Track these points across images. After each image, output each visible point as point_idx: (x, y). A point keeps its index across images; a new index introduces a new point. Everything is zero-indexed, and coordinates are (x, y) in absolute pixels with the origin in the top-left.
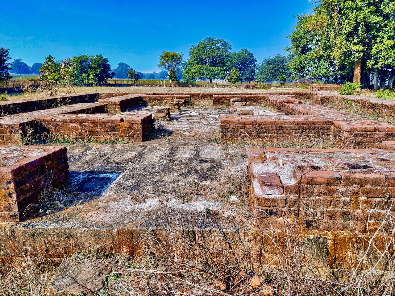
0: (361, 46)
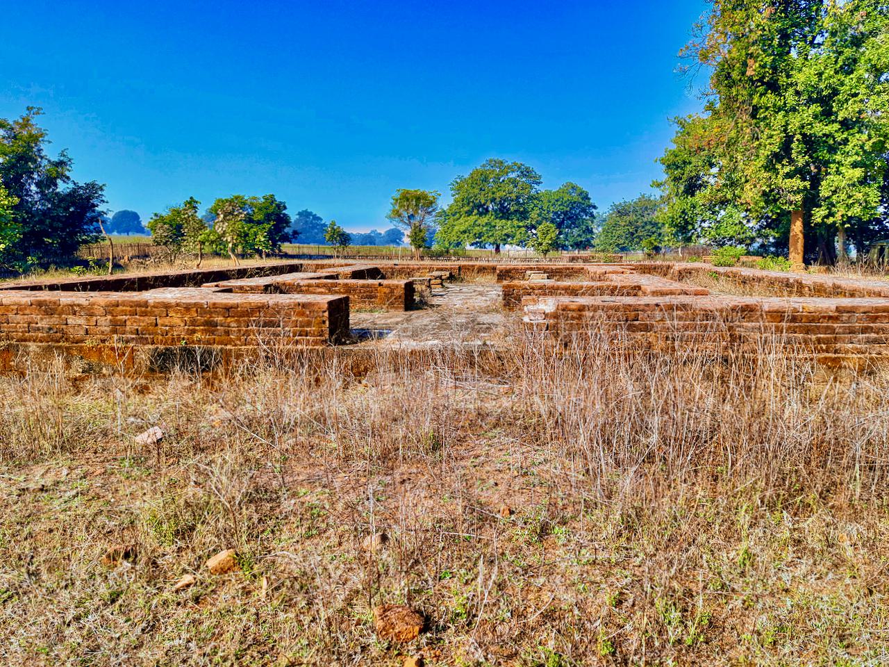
0: (799, 181)
